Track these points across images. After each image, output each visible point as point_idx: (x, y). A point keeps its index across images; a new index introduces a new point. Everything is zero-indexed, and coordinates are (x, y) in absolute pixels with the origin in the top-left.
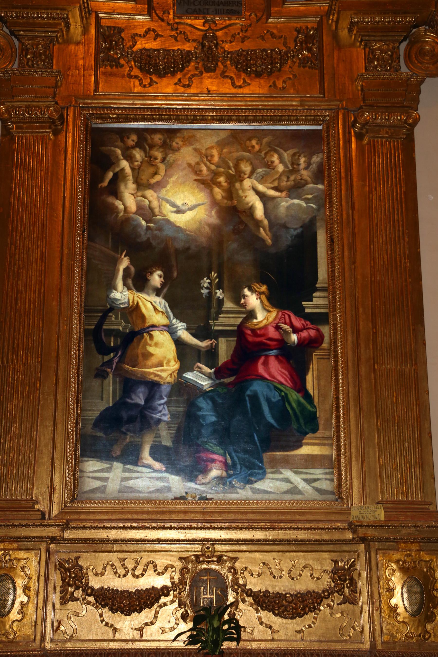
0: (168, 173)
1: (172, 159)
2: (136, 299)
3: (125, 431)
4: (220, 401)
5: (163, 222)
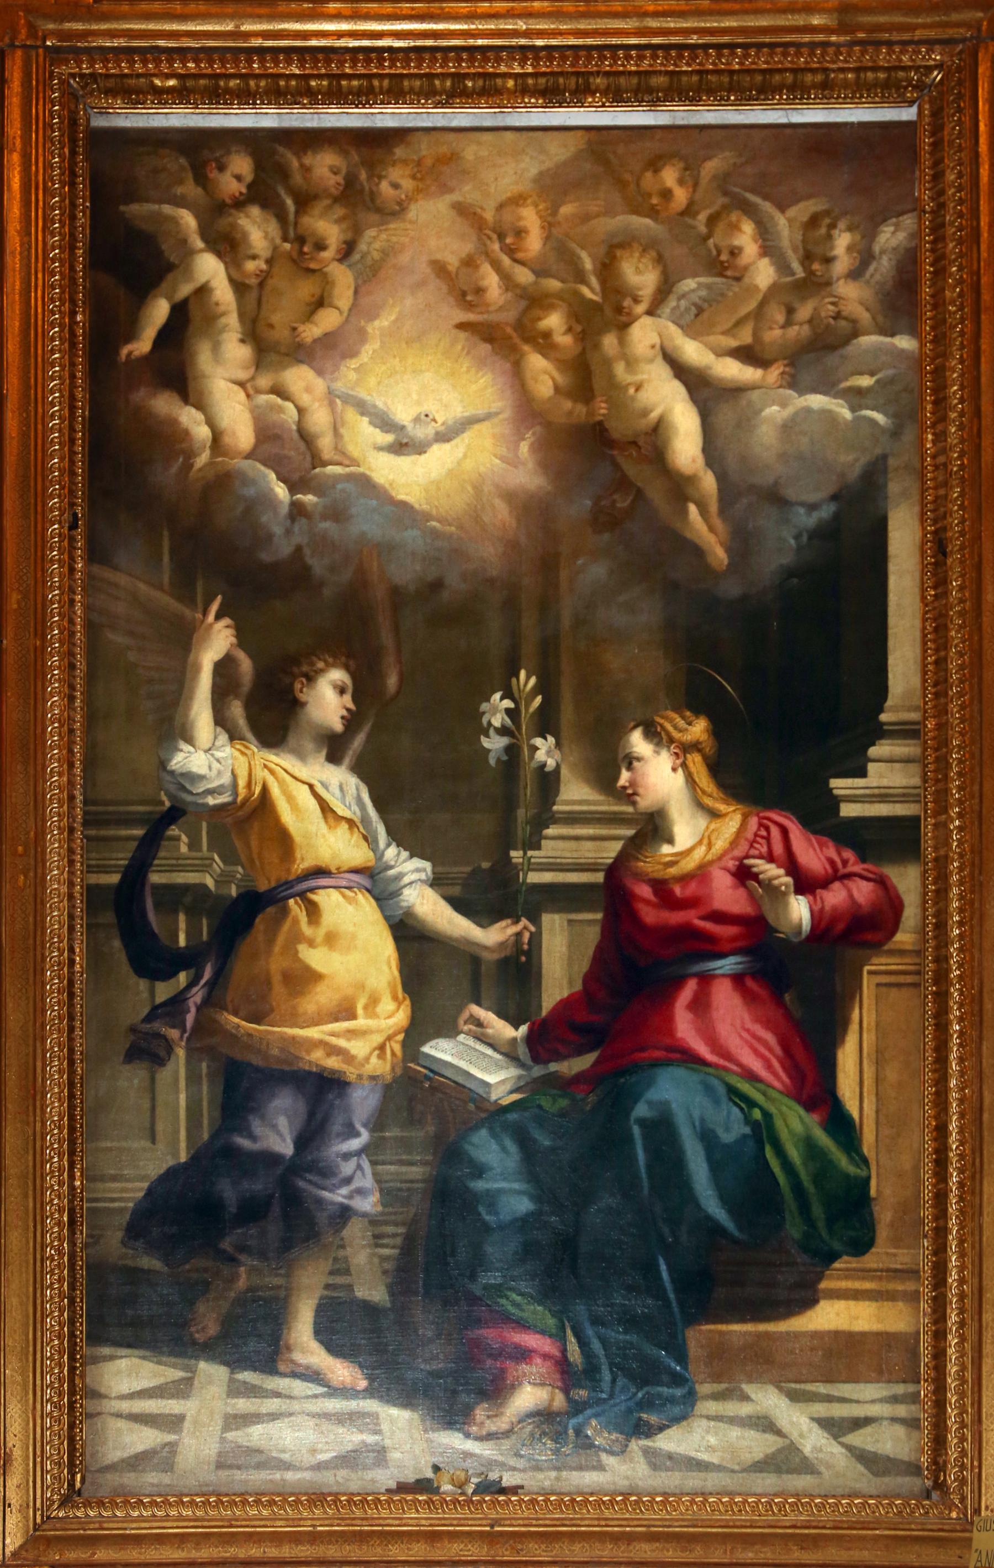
0: (365, 301)
1: (377, 245)
2: (261, 774)
3: (230, 1249)
4: (545, 1141)
5: (350, 487)
